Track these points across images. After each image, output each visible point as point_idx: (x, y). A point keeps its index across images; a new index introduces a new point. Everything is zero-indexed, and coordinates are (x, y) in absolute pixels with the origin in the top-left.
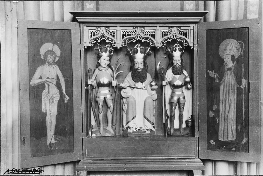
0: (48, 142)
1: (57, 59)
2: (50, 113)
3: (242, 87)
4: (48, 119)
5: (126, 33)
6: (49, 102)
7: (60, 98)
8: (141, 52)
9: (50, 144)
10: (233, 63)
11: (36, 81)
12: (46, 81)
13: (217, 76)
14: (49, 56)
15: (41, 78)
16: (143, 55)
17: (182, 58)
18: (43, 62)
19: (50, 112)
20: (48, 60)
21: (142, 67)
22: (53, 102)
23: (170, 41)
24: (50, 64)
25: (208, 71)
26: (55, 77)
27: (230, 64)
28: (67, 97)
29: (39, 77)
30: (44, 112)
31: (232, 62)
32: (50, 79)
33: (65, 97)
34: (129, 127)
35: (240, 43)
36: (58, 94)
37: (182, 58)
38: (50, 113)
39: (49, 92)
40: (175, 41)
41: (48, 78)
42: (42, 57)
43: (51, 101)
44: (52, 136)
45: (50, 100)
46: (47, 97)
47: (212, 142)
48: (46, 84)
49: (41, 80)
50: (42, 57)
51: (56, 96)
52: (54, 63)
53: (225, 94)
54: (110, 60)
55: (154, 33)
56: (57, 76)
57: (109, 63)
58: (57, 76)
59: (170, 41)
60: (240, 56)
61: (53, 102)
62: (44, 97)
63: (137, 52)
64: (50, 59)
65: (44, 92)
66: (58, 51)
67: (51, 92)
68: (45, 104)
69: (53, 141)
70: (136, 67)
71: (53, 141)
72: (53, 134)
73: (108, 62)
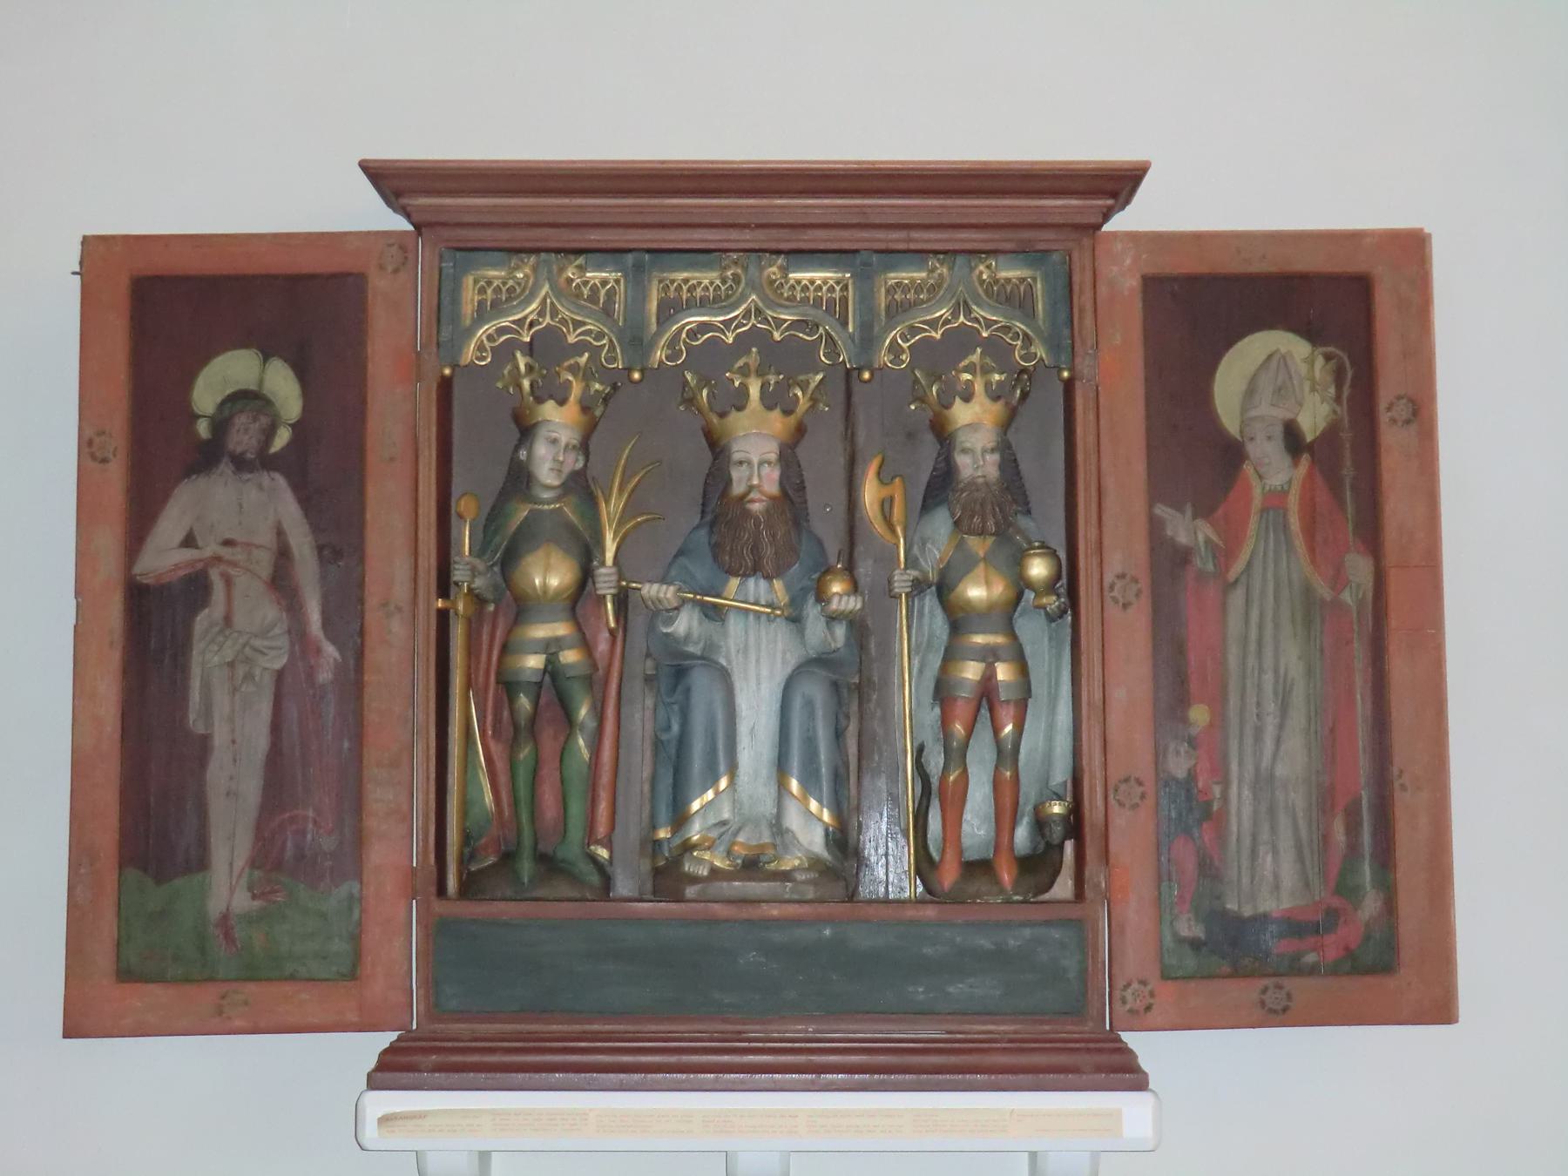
0: (215, 907)
1: (282, 438)
2: (234, 742)
3: (1347, 597)
4: (218, 773)
5: (679, 288)
6: (232, 678)
7: (275, 470)
8: (770, 400)
9: (225, 917)
10: (1296, 463)
11: (163, 556)
12: (218, 559)
13: (1208, 541)
14: (241, 420)
15: (189, 542)
16: (777, 423)
17: (1011, 436)
18: (207, 456)
19: (233, 731)
20: (231, 446)
21: (772, 488)
22: (249, 677)
23: (938, 336)
24: (241, 464)
25: (1161, 510)
26: (266, 538)
27: (1272, 470)
28: (330, 650)
29: (180, 536)
30: (200, 729)
31: (1286, 460)
32: (238, 549)
33: (319, 651)
34: (687, 847)
35: (1328, 358)
36: (277, 631)
37: (1011, 436)
38: (234, 742)
39: (228, 619)
40: (960, 341)
41: (228, 543)
42: (203, 429)
43: (241, 671)
44: (236, 873)
45: (231, 665)
46: (221, 647)
47: (1190, 928)
48: (215, 575)
49: (188, 554)
50: (203, 429)
51: (266, 643)
52: (266, 462)
53: (1253, 647)
54: (584, 447)
55: (845, 288)
56: (280, 533)
57: (580, 465)
58: (280, 533)
59: (938, 336)
60: (1331, 434)
61: (253, 677)
62: (202, 645)
63: (739, 400)
64: (243, 438)
65: (201, 621)
66: (284, 389)
67: (239, 620)
68: (206, 688)
69: (242, 902)
70: (738, 489)
71: (242, 902)
72: (240, 863)
73: (574, 462)
